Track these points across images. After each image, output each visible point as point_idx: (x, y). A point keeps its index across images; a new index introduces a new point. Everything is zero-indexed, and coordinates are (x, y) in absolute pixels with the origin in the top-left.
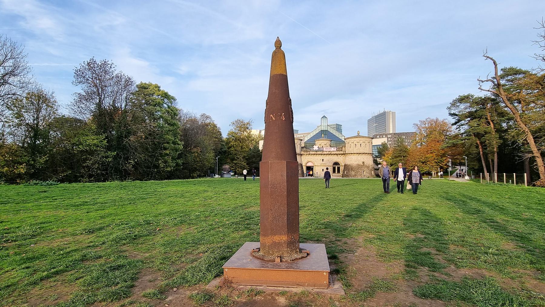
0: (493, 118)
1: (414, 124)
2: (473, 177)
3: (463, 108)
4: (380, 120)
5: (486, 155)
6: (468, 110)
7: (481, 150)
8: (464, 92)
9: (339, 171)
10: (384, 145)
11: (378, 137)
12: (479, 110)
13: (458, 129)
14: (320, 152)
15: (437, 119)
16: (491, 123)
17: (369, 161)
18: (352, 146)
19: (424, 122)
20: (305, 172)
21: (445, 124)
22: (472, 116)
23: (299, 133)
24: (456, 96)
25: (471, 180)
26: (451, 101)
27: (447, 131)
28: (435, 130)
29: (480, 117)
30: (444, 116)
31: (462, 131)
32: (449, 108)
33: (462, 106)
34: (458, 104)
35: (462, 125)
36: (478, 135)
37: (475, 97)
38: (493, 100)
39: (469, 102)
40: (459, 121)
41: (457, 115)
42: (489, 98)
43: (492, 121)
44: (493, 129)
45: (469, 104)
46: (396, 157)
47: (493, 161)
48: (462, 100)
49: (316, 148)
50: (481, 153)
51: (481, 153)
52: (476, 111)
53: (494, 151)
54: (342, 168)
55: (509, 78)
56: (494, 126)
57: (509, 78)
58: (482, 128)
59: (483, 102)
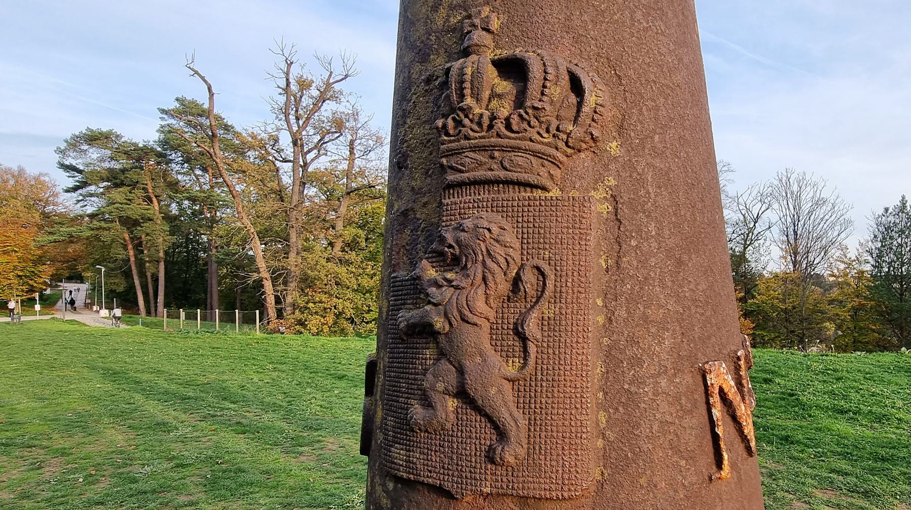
3: (94, 157)
6: (107, 165)
7: (131, 253)
12: (129, 170)
13: (81, 204)
15: (21, 171)
16: (154, 199)
21: (39, 183)
22: (116, 179)
24: (80, 127)
26: (68, 136)
27: (47, 203)
29: (134, 185)
30: (43, 165)
31: (90, 210)
32: (62, 152)
33: (94, 154)
34: (85, 147)
35: (91, 195)
36: (130, 223)
37: (123, 140)
38: (160, 155)
40: (84, 184)
41: (80, 172)
42: (152, 150)
43: (156, 196)
44: (157, 213)
45: (108, 152)
47: (156, 280)
48: (94, 138)
50: (132, 259)
51: (132, 259)
52: (123, 171)
53: (159, 257)
56: (160, 208)
58: (136, 209)
59: (138, 154)
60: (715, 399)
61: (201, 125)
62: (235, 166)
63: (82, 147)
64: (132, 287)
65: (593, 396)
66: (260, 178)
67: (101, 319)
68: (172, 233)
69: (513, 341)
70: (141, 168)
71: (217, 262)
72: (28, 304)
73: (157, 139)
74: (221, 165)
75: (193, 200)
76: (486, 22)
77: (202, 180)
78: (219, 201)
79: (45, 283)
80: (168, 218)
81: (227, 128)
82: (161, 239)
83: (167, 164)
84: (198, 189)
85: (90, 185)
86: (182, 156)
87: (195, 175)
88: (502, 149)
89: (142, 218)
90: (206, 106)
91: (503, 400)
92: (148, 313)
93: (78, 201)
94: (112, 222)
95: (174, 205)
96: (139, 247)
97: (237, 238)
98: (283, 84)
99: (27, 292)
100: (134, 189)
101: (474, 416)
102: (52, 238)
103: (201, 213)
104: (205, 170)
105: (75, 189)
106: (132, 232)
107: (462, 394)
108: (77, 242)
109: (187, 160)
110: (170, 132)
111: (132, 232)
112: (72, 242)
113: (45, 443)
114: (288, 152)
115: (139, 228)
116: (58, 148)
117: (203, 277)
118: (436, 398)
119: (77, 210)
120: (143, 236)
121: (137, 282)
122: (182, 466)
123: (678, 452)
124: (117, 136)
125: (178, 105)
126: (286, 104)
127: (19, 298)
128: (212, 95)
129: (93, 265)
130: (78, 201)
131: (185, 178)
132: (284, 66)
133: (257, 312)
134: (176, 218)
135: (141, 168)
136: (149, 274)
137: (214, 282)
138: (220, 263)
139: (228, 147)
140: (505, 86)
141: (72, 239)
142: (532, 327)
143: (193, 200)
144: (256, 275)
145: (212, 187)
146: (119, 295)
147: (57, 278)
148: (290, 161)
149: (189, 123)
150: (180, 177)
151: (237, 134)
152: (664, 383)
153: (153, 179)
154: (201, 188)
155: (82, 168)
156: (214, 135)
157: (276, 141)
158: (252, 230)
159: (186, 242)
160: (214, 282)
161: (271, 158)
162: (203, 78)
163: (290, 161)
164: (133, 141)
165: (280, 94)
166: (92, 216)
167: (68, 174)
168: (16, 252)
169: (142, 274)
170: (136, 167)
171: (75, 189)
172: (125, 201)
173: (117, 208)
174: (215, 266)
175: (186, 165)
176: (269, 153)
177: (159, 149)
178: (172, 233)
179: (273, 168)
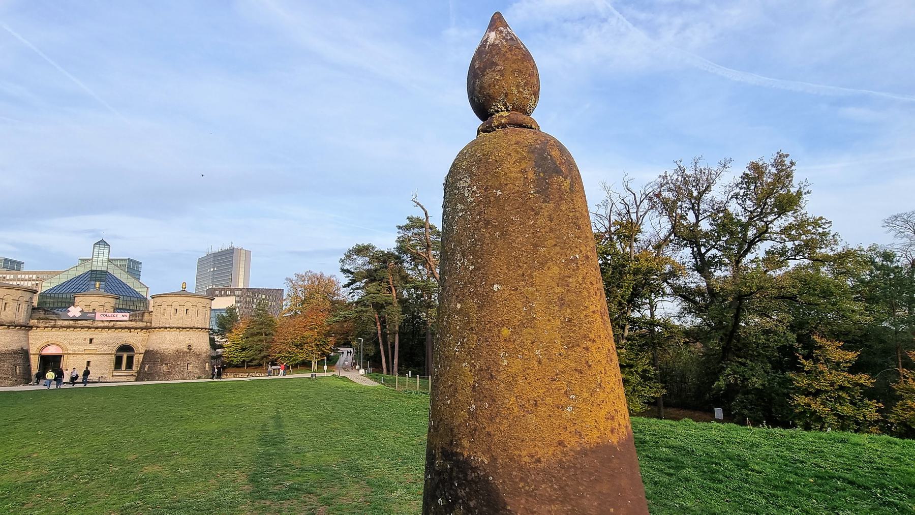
1: (287, 279)
4: (223, 262)
5: (384, 335)
6: (366, 267)
7: (379, 328)
9: (129, 366)
10: (230, 311)
11: (217, 292)
12: (379, 269)
14: (87, 321)
15: (322, 274)
17: (201, 343)
18: (167, 312)
19: (301, 277)
20: (35, 370)
21: (331, 282)
22: (371, 277)
23: (25, 268)
24: (352, 245)
25: (368, 375)
27: (334, 295)
28: (316, 292)
29: (381, 280)
31: (356, 298)
33: (360, 261)
34: (355, 257)
35: (357, 289)
36: (379, 307)
38: (398, 258)
40: (353, 282)
41: (352, 273)
45: (368, 259)
46: (253, 335)
47: (393, 347)
48: (361, 251)
49: (74, 312)
52: (376, 270)
54: (138, 359)
55: (416, 231)
57: (416, 231)
58: (383, 296)
59: (384, 259)
70: (386, 268)
72: (320, 364)
80: (402, 302)
105: (349, 285)
110: (403, 241)
141: (346, 319)
147: (337, 345)
150: (409, 272)
162: (422, 207)
166: (357, 303)
171: (349, 285)
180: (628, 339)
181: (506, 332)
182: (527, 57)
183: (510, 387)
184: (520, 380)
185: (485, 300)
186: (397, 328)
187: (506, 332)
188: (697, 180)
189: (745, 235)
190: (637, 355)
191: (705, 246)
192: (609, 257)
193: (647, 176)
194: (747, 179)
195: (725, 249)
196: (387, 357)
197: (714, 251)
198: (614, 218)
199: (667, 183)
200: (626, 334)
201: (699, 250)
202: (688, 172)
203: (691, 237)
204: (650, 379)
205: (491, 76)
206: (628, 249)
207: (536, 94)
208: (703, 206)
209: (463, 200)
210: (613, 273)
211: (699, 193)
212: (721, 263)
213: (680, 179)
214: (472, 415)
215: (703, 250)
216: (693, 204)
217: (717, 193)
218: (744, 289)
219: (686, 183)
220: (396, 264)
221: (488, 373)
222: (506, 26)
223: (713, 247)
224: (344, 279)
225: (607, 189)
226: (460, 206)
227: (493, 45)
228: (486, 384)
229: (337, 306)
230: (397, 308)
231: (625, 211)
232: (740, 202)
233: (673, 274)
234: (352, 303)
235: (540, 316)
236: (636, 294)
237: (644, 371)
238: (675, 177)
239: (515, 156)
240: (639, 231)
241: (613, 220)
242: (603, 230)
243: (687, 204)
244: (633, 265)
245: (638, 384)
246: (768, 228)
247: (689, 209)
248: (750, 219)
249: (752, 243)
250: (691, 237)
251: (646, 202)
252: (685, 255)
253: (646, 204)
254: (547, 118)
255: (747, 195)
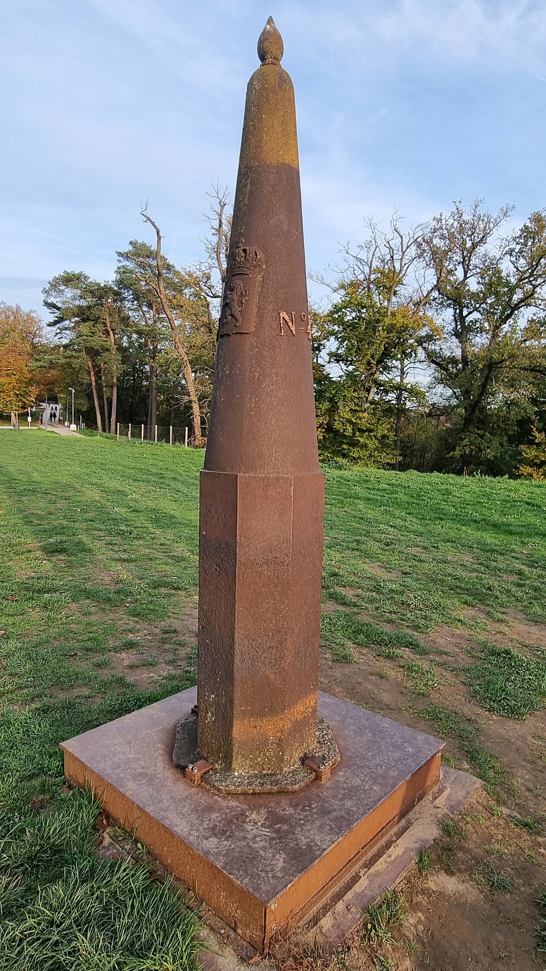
0: (114, 325)
2: (83, 425)
3: (69, 296)
6: (77, 303)
7: (93, 379)
8: (74, 268)
12: (93, 306)
13: (59, 336)
15: (18, 308)
16: (111, 333)
21: (30, 319)
22: (84, 315)
24: (59, 272)
25: (80, 431)
27: (35, 336)
29: (96, 320)
31: (65, 341)
33: (69, 293)
34: (62, 288)
35: (66, 329)
36: (93, 353)
37: (89, 281)
38: (117, 294)
39: (80, 288)
40: (61, 320)
41: (58, 309)
42: (111, 289)
43: (112, 330)
44: (113, 344)
47: (110, 403)
48: (69, 280)
50: (94, 384)
51: (94, 384)
52: (89, 308)
56: (115, 340)
58: (97, 341)
59: (100, 293)
60: (281, 319)
61: (150, 266)
62: (175, 301)
63: (60, 288)
64: (93, 408)
65: (254, 314)
66: (194, 312)
67: (70, 431)
68: (123, 362)
69: (240, 304)
70: (102, 305)
71: (156, 389)
72: (23, 417)
73: (114, 279)
74: (164, 300)
75: (140, 333)
76: (242, 241)
77: (147, 316)
78: (160, 334)
79: (32, 401)
80: (120, 349)
81: (169, 267)
82: (115, 368)
83: (121, 301)
84: (144, 323)
85: (66, 320)
86: (133, 294)
87: (142, 311)
88: (242, 267)
89: (102, 349)
90: (154, 248)
91: (238, 315)
92: (104, 430)
93: (57, 334)
94: (80, 351)
95: (125, 338)
96: (98, 374)
97: (173, 366)
98: (216, 225)
99: (21, 408)
100: (96, 323)
101: (233, 318)
102: (38, 364)
103: (146, 346)
104: (150, 306)
105: (55, 323)
106: (94, 361)
107: (232, 315)
108: (55, 368)
109: (137, 298)
110: (124, 272)
111: (94, 361)
112: (51, 368)
113: (54, 493)
114: (217, 289)
115: (99, 358)
116: (44, 289)
117: (146, 403)
118: (227, 316)
119: (56, 341)
120: (102, 365)
121: (96, 404)
122: (137, 511)
123: (271, 328)
124: (85, 277)
125: (131, 248)
126: (218, 244)
127: (17, 412)
128: (159, 238)
129: (66, 388)
130: (57, 334)
131: (134, 314)
132: (218, 208)
133: (187, 428)
134: (126, 350)
135: (102, 305)
136: (105, 397)
137: (154, 406)
138: (159, 390)
139: (170, 285)
140: (243, 254)
141: (52, 365)
142: (244, 301)
143: (140, 333)
144: (187, 397)
145: (155, 322)
146: (83, 413)
147: (40, 399)
148: (218, 297)
149: (141, 265)
150: (130, 314)
151: (177, 273)
152: (269, 314)
153: (110, 315)
154: (146, 322)
155: (60, 305)
156: (160, 274)
157: (208, 278)
158: (186, 359)
159: (133, 371)
160: (154, 406)
161: (203, 294)
162: (153, 224)
163: (218, 297)
164: (97, 282)
165: (214, 234)
166: (66, 347)
167: (50, 311)
168: (15, 375)
169: (100, 398)
170: (98, 305)
171: (55, 323)
172: (90, 334)
173: (84, 340)
174: (155, 392)
175: (135, 302)
176: (201, 289)
177: (116, 288)
178: (123, 362)
179: (204, 303)
180: (372, 403)
181: (266, 129)
182: (280, 38)
183: (266, 144)
184: (269, 142)
185: (261, 120)
186: (115, 380)
187: (266, 129)
188: (473, 228)
189: (510, 299)
190: (379, 419)
191: (468, 308)
192: (364, 311)
193: (421, 214)
194: (527, 233)
195: (488, 314)
196: (102, 415)
197: (476, 315)
198: (376, 264)
199: (441, 228)
200: (370, 398)
201: (461, 312)
202: (466, 217)
203: (456, 298)
204: (387, 446)
205: (267, 44)
206: (386, 303)
207: (282, 53)
208: (475, 261)
209: (255, 89)
210: (366, 328)
211: (473, 244)
212: (482, 330)
213: (456, 224)
214: (255, 153)
215: (465, 313)
216: (464, 258)
217: (491, 248)
218: (495, 356)
219: (461, 231)
220: (115, 301)
221: (260, 141)
222: (273, 23)
223: (476, 309)
224: (49, 316)
225: (372, 226)
226: (254, 91)
227: (268, 31)
228: (259, 144)
229: (37, 350)
230: (115, 356)
231: (388, 257)
232: (513, 259)
233: (429, 338)
234: (59, 347)
235: (276, 126)
236: (386, 354)
237: (384, 437)
238: (451, 221)
239: (272, 74)
240: (400, 282)
241: (374, 266)
242: (361, 277)
243: (458, 257)
244: (387, 321)
245: (375, 450)
246: (534, 292)
247: (459, 263)
248: (520, 280)
249: (517, 307)
250: (456, 298)
251: (413, 247)
252: (446, 317)
253: (413, 251)
254: (284, 63)
255: (522, 251)
